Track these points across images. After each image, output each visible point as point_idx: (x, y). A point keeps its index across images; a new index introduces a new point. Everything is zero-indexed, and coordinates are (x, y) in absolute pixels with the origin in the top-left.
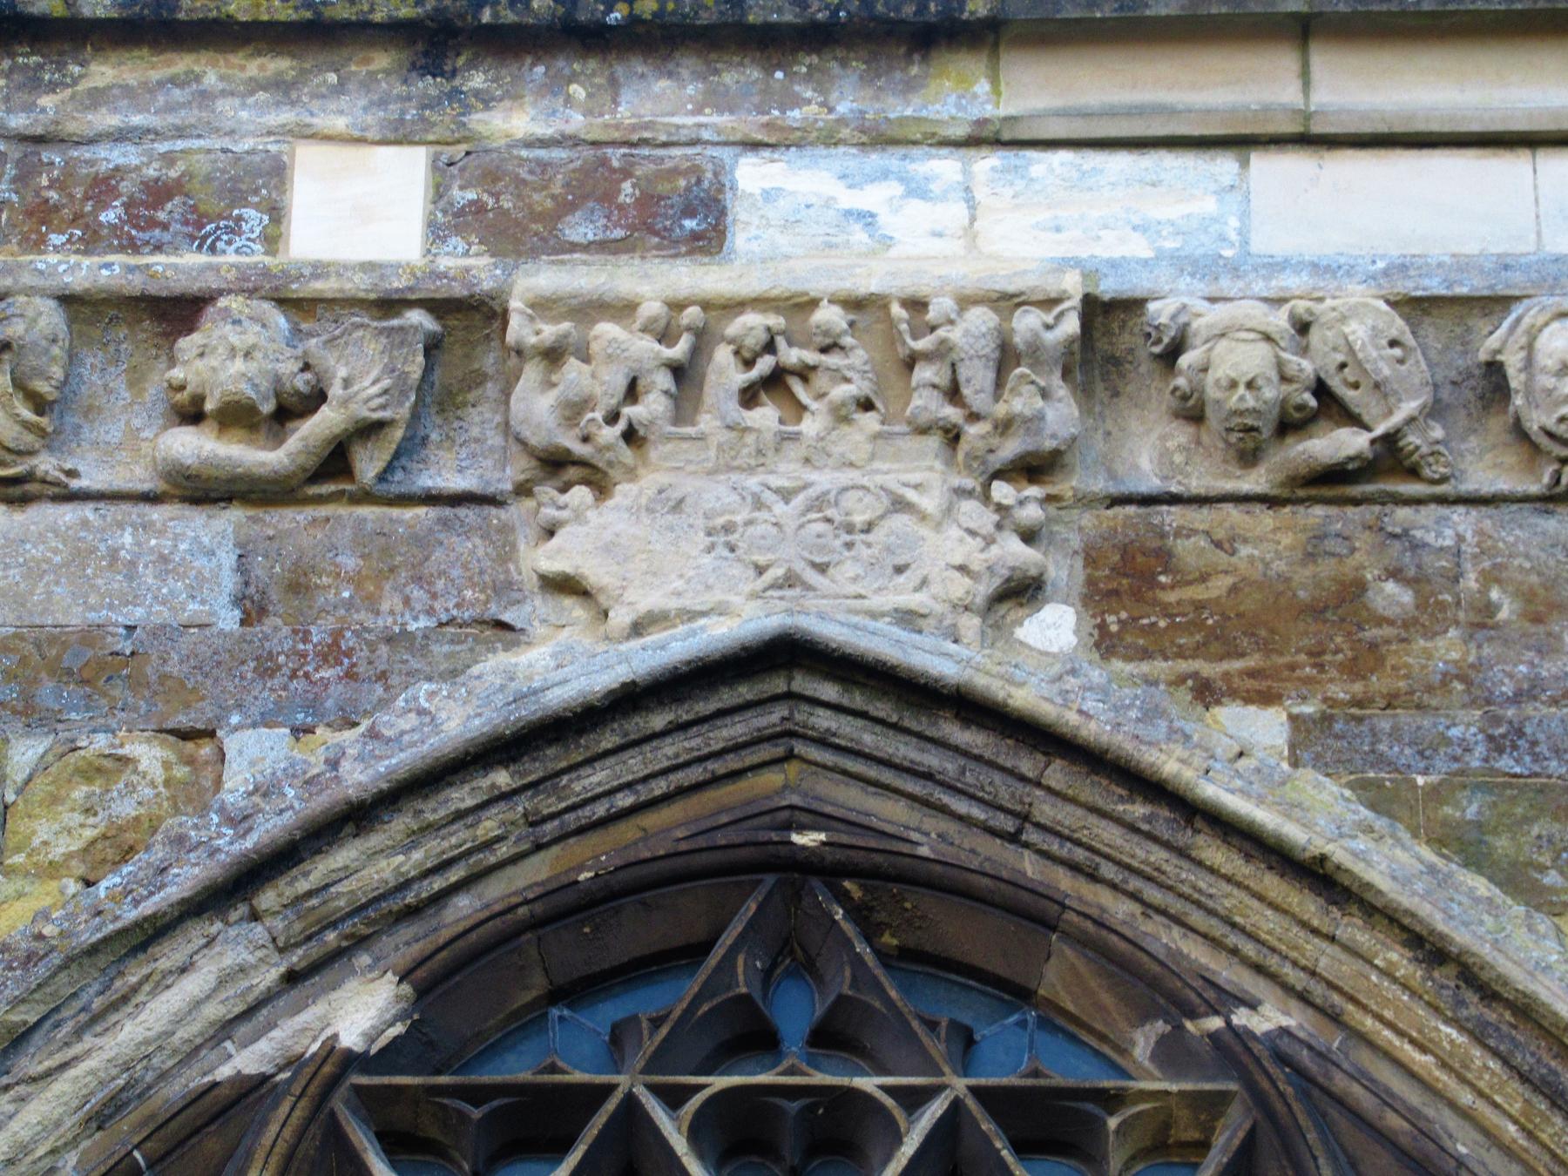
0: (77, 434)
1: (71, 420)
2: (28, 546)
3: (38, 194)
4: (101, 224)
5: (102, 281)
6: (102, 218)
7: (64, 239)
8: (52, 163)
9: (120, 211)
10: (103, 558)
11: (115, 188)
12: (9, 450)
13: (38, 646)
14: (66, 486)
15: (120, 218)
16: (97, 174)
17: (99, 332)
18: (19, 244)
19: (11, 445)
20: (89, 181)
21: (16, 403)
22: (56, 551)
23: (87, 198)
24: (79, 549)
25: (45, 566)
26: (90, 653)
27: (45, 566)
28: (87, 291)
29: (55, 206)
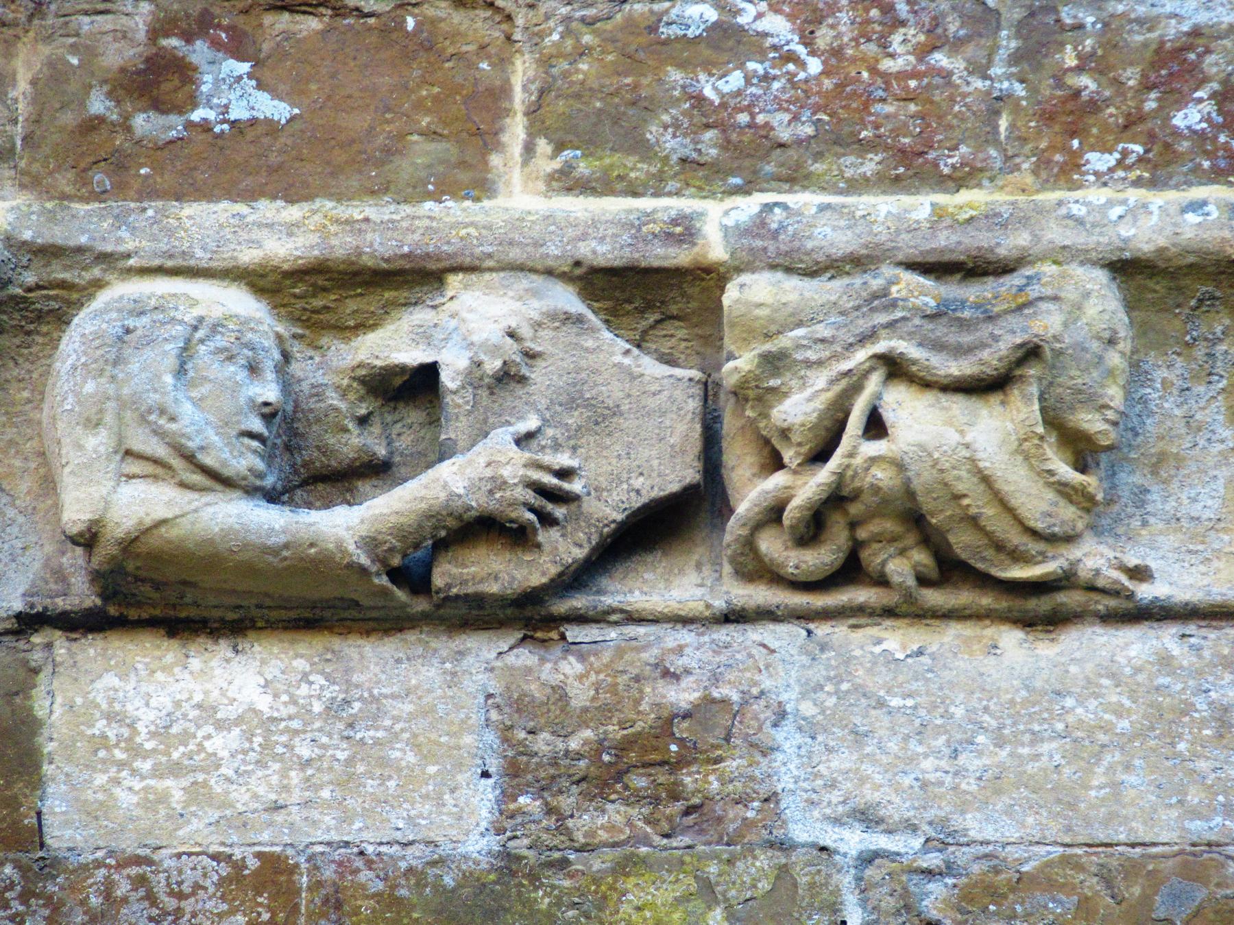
0: (1141, 504)
1: (1130, 479)
2: (1069, 702)
3: (1059, 82)
4: (1176, 133)
5: (1188, 234)
6: (1179, 121)
7: (1111, 159)
8: (1080, 27)
9: (1209, 107)
10: (1203, 723)
11: (1194, 67)
12: (1034, 533)
13: (1108, 883)
14: (1131, 596)
15: (1208, 119)
16: (1162, 43)
17: (1177, 323)
18: (1035, 172)
19: (1039, 525)
20: (1148, 54)
21: (1050, 453)
22: (1119, 712)
23: (1147, 86)
24: (1159, 707)
25: (1102, 738)
26: (1201, 894)
27: (1102, 738)
28: (1161, 251)
29: (1092, 102)
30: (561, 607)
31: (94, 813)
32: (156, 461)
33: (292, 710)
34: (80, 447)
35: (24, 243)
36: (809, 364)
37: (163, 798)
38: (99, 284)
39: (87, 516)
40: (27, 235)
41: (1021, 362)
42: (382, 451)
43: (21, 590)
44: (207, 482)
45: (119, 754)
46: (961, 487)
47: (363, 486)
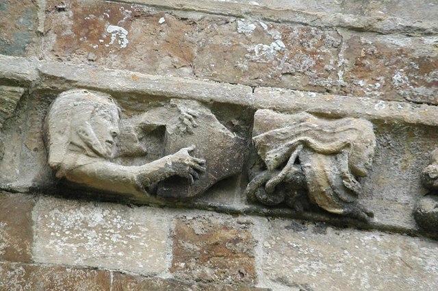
2: (346, 252)
30: (200, 202)
31: (47, 252)
32: (81, 147)
33: (111, 226)
34: (57, 139)
35: (44, 74)
36: (280, 140)
37: (71, 249)
38: (65, 90)
39: (58, 161)
40: (46, 72)
41: (344, 148)
42: (145, 150)
43: (31, 180)
44: (95, 155)
45: (58, 235)
46: (321, 183)
47: (137, 160)
